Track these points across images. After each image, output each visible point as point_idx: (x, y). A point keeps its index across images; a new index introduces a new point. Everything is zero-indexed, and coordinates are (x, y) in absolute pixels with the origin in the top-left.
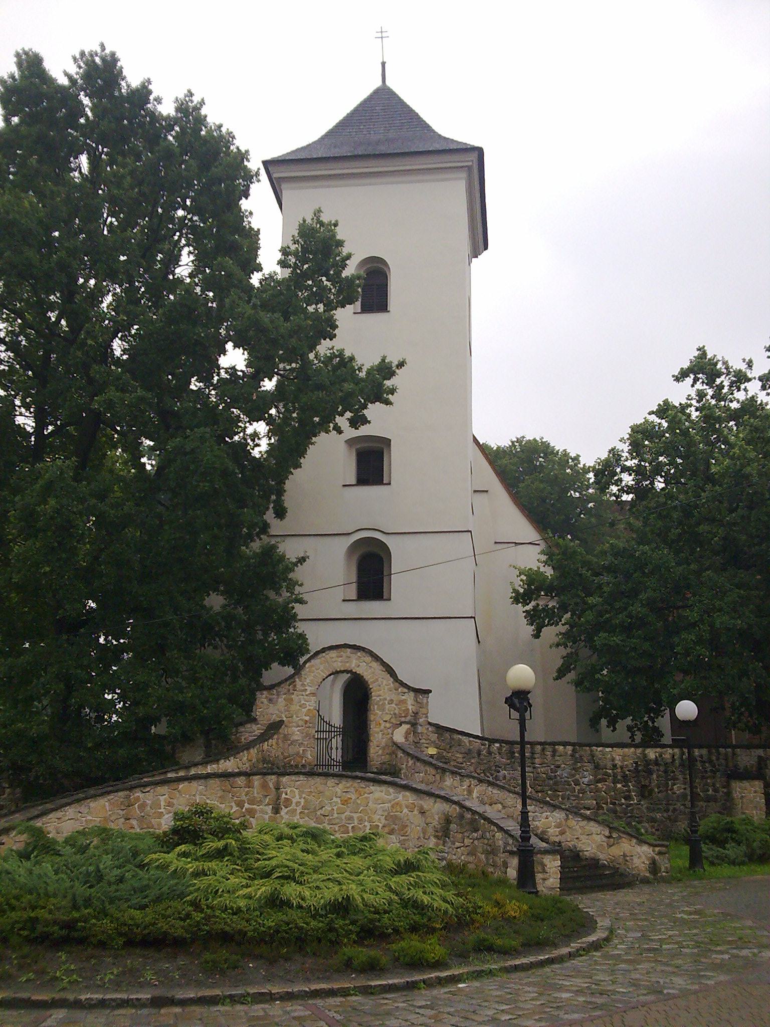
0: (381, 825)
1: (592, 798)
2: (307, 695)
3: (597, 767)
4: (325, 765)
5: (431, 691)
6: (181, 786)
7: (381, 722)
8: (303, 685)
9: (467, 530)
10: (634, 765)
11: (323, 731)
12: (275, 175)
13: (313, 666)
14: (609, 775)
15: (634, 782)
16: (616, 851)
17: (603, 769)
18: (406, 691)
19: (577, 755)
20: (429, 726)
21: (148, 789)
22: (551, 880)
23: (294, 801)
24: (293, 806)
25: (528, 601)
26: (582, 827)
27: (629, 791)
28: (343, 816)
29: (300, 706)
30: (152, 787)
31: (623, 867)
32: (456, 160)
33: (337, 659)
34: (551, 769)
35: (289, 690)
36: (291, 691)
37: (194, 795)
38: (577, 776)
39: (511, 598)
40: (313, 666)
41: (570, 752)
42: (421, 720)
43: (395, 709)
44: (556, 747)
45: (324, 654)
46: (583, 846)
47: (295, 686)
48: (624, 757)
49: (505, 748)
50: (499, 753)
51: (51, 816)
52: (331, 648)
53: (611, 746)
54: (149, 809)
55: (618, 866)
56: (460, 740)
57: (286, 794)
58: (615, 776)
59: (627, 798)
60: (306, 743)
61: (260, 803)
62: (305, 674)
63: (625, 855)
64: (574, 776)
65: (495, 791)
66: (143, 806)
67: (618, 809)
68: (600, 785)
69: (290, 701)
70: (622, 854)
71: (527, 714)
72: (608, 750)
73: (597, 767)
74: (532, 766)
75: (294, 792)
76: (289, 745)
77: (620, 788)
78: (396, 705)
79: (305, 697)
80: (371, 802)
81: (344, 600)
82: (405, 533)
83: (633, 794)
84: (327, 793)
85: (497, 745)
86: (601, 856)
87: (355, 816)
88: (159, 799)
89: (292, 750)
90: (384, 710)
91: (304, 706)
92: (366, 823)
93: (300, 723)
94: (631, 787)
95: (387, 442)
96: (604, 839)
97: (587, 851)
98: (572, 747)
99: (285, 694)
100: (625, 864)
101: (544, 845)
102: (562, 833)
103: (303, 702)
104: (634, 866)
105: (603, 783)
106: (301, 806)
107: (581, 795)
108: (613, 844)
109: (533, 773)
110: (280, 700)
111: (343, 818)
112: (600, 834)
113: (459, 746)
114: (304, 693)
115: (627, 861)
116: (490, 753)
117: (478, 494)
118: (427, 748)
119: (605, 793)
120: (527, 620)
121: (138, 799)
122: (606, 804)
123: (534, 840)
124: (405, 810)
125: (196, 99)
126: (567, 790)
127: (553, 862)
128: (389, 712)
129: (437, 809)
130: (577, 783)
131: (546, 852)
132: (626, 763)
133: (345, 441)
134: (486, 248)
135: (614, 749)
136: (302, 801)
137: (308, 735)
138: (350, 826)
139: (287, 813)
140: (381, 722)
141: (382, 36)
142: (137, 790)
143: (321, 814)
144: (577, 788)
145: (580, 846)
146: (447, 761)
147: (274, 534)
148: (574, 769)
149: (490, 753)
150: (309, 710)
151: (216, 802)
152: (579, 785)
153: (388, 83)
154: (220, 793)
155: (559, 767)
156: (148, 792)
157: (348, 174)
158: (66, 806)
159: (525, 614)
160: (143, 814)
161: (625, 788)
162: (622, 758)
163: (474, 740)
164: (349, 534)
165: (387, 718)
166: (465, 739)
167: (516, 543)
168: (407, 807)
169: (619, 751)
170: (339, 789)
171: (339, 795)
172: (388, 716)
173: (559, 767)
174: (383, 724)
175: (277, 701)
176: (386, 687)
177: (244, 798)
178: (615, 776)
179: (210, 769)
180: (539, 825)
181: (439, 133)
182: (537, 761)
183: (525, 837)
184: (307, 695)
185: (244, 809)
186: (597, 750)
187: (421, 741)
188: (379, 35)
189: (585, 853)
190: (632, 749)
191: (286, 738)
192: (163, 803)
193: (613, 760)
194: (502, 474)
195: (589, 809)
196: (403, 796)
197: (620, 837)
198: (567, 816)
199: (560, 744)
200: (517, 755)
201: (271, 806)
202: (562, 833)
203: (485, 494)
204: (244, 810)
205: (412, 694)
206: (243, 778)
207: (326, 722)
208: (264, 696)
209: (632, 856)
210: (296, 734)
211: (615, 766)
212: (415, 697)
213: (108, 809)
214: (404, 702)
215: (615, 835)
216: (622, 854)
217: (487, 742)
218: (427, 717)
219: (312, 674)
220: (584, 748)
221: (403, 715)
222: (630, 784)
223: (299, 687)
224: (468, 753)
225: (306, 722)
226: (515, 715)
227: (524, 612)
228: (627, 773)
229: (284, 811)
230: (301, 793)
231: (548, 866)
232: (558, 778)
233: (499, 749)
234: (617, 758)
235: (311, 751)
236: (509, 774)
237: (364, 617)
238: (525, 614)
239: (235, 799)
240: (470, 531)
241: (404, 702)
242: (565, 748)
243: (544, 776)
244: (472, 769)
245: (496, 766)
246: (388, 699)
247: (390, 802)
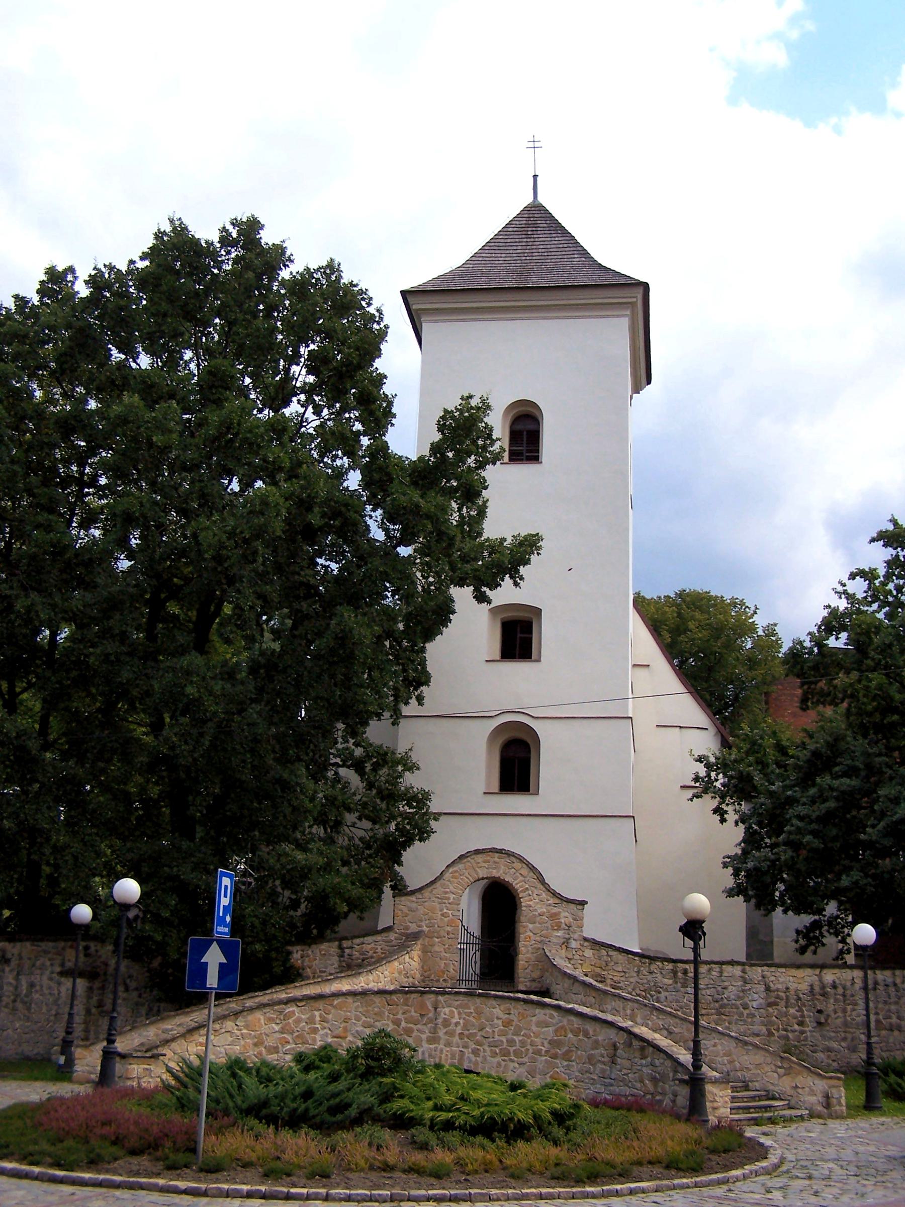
1: (763, 1024)
3: (768, 989)
5: (586, 903)
6: (336, 1002)
12: (414, 307)
24: (452, 1027)
27: (803, 1016)
33: (484, 864)
34: (717, 991)
38: (746, 1000)
52: (478, 852)
59: (801, 1024)
67: (790, 1035)
71: (701, 943)
73: (768, 989)
81: (485, 793)
92: (529, 1047)
101: (715, 1073)
103: (445, 911)
122: (778, 1030)
123: (705, 1068)
124: (570, 1035)
129: (605, 1035)
130: (745, 1007)
131: (715, 1082)
134: (649, 382)
136: (462, 1021)
141: (534, 145)
144: (746, 1012)
155: (725, 988)
167: (681, 727)
168: (571, 1031)
173: (725, 988)
181: (600, 262)
183: (697, 1065)
188: (531, 145)
192: (318, 1018)
194: (655, 627)
195: (758, 1035)
196: (569, 1020)
203: (646, 669)
218: (582, 931)
226: (690, 943)
230: (459, 1013)
240: (631, 718)
243: (710, 998)
247: (554, 1025)
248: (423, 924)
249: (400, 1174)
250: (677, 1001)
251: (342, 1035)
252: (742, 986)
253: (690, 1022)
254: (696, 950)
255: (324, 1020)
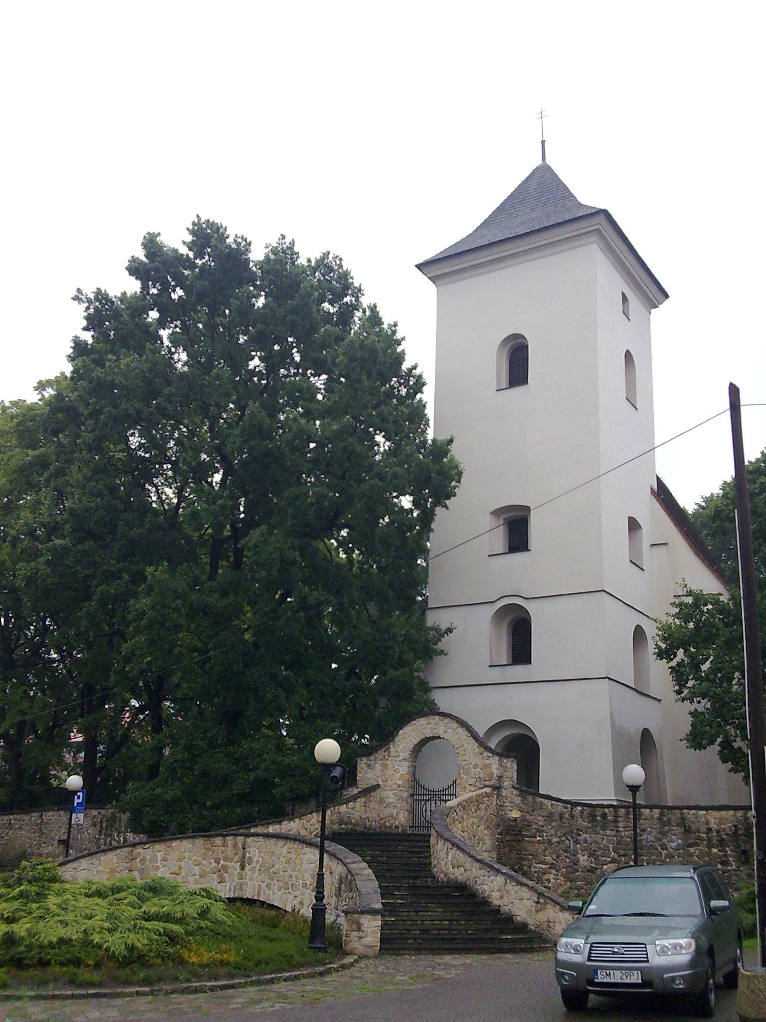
0: (309, 883)
2: (400, 761)
3: (688, 831)
4: (418, 827)
6: (174, 844)
7: (467, 786)
8: (397, 751)
9: (601, 589)
10: (733, 828)
11: (451, 795)
13: (405, 733)
14: (702, 839)
15: (732, 847)
16: (542, 917)
17: (695, 833)
18: (490, 755)
19: (665, 819)
20: (513, 789)
21: (147, 846)
22: (369, 939)
23: (255, 859)
24: (254, 864)
25: (672, 657)
26: (516, 892)
27: (726, 856)
28: (286, 874)
29: (394, 771)
30: (151, 844)
31: (546, 933)
32: (584, 226)
35: (384, 757)
36: (387, 757)
37: (184, 852)
38: (665, 841)
39: (654, 654)
40: (405, 733)
41: (657, 816)
42: (505, 784)
43: (480, 773)
44: (642, 810)
45: (415, 722)
46: (516, 911)
47: (389, 752)
48: (721, 821)
49: (588, 810)
50: (581, 816)
51: (68, 866)
53: (706, 808)
54: (148, 862)
55: (542, 931)
56: (542, 803)
57: (250, 853)
58: (709, 840)
59: (725, 863)
60: (398, 805)
61: (231, 860)
62: (399, 741)
63: (549, 921)
64: (659, 840)
65: (461, 855)
66: (143, 861)
68: (692, 850)
69: (385, 766)
70: (546, 920)
72: (702, 812)
73: (688, 831)
74: (615, 829)
75: (255, 851)
76: (385, 807)
77: (715, 853)
78: (481, 769)
79: (398, 762)
80: (304, 863)
81: (490, 666)
82: (454, 606)
83: (731, 859)
84: (277, 853)
85: (580, 808)
86: (530, 921)
87: (294, 874)
88: (156, 855)
89: (386, 812)
90: (469, 774)
91: (397, 771)
93: (394, 787)
94: (729, 852)
95: (528, 509)
96: (534, 904)
97: (519, 915)
98: (660, 811)
99: (381, 760)
100: (548, 930)
102: (501, 897)
103: (397, 767)
104: (556, 933)
105: (695, 848)
106: (259, 865)
107: (668, 860)
108: (541, 910)
109: (616, 836)
110: (376, 766)
111: (286, 876)
112: (530, 899)
113: (542, 809)
114: (397, 759)
115: (549, 927)
116: (572, 816)
117: (655, 547)
118: (511, 811)
119: (698, 858)
120: (673, 677)
121: (139, 854)
125: (288, 241)
126: (653, 854)
127: (372, 922)
128: (474, 776)
130: (664, 847)
132: (723, 826)
133: (491, 513)
135: (710, 812)
136: (260, 859)
137: (401, 798)
138: (290, 883)
139: (249, 870)
140: (467, 786)
142: (139, 846)
143: (273, 872)
145: (514, 911)
146: (530, 824)
147: (432, 607)
148: (661, 833)
149: (572, 816)
150: (402, 774)
151: (200, 859)
152: (666, 849)
153: (548, 161)
154: (203, 851)
156: (148, 848)
157: (500, 258)
158: (80, 859)
159: (670, 670)
160: (143, 867)
161: (721, 853)
162: (719, 822)
163: (556, 803)
164: (493, 602)
165: (472, 781)
166: (548, 803)
169: (715, 813)
170: (285, 850)
171: (284, 855)
172: (473, 779)
174: (468, 788)
175: (374, 766)
176: (472, 752)
177: (221, 856)
178: (709, 840)
179: (272, 829)
180: (486, 888)
182: (620, 824)
184: (400, 761)
185: (220, 865)
186: (688, 813)
187: (505, 804)
189: (518, 917)
190: (732, 812)
191: (381, 801)
192: (159, 859)
193: (708, 823)
197: (546, 903)
198: (506, 880)
199: (690, 808)
200: (599, 818)
201: (239, 863)
202: (501, 897)
204: (220, 866)
205: (496, 758)
206: (220, 838)
207: (421, 786)
208: (363, 762)
209: (555, 922)
210: (390, 796)
211: (709, 830)
212: (500, 761)
213: (115, 862)
214: (489, 766)
215: (542, 901)
216: (546, 920)
217: (569, 806)
219: (405, 741)
220: (673, 811)
221: (487, 779)
222: (727, 849)
223: (392, 753)
224: (550, 817)
225: (399, 786)
227: (669, 668)
228: (725, 837)
229: (247, 868)
230: (260, 852)
231: (365, 926)
232: (644, 842)
233: (581, 812)
234: (713, 821)
235: (403, 813)
236: (591, 837)
237: (509, 681)
238: (670, 670)
239: (214, 856)
241: (489, 766)
242: (652, 811)
244: (553, 832)
245: (578, 830)
246: (473, 763)
248: (380, 780)
249: (57, 969)
250: (596, 842)
251: (177, 871)
252: (660, 828)
253: (327, 852)
254: (634, 799)
255: (164, 859)
